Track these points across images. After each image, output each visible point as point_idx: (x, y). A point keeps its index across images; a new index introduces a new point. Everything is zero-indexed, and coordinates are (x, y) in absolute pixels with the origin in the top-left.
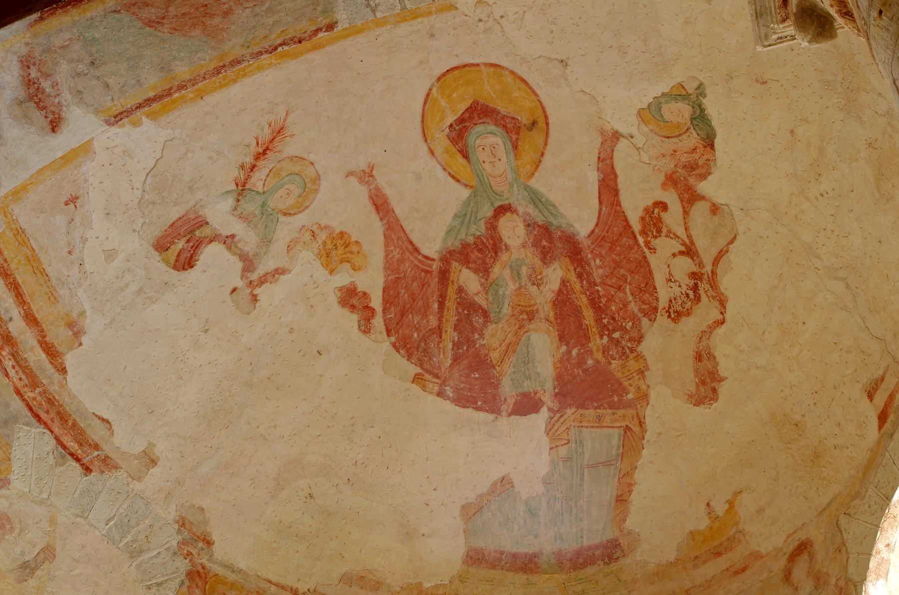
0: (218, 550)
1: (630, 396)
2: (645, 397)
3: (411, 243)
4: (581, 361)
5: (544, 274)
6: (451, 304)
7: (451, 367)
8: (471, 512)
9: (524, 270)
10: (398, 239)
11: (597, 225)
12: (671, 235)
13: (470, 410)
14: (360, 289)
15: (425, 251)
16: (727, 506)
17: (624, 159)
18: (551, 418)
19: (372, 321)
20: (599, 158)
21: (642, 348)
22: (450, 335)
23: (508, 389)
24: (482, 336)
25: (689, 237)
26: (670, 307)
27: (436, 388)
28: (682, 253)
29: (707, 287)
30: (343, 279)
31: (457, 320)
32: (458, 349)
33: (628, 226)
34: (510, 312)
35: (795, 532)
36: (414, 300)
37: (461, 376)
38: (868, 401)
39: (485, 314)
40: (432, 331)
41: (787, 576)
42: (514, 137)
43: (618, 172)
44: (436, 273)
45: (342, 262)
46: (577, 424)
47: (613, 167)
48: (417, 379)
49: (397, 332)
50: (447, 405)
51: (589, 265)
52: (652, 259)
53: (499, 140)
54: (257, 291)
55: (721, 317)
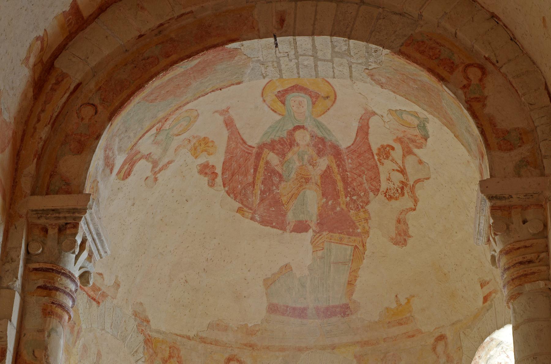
0: (153, 324)
1: (359, 231)
2: (367, 232)
3: (242, 139)
4: (333, 208)
5: (318, 161)
6: (261, 170)
7: (259, 204)
8: (269, 283)
9: (306, 157)
10: (235, 138)
11: (353, 144)
12: (393, 160)
13: (269, 227)
14: (211, 164)
15: (250, 143)
16: (406, 301)
17: (374, 122)
18: (315, 236)
19: (216, 180)
20: (361, 118)
21: (368, 207)
22: (259, 186)
23: (290, 217)
24: (277, 188)
25: (404, 166)
26: (386, 192)
27: (250, 215)
28: (398, 171)
29: (409, 191)
30: (202, 160)
31: (264, 179)
32: (264, 194)
33: (370, 148)
34: (295, 177)
35: (439, 328)
36: (240, 167)
37: (264, 209)
38: (480, 288)
39: (280, 176)
40: (249, 184)
41: (434, 349)
42: (314, 100)
43: (370, 126)
44: (254, 154)
45: (202, 151)
46: (328, 240)
47: (368, 124)
48: (239, 210)
49: (229, 185)
50: (257, 225)
51: (344, 161)
52: (381, 168)
53: (305, 100)
54: (158, 175)
55: (414, 207)
